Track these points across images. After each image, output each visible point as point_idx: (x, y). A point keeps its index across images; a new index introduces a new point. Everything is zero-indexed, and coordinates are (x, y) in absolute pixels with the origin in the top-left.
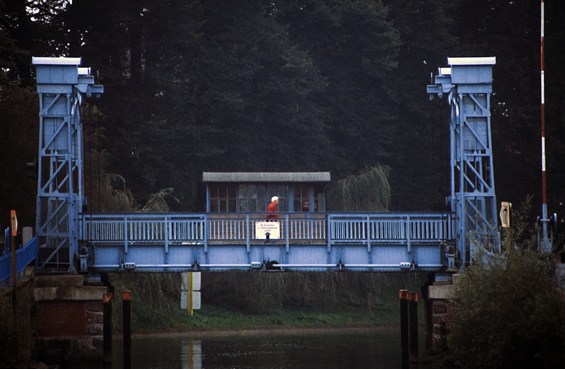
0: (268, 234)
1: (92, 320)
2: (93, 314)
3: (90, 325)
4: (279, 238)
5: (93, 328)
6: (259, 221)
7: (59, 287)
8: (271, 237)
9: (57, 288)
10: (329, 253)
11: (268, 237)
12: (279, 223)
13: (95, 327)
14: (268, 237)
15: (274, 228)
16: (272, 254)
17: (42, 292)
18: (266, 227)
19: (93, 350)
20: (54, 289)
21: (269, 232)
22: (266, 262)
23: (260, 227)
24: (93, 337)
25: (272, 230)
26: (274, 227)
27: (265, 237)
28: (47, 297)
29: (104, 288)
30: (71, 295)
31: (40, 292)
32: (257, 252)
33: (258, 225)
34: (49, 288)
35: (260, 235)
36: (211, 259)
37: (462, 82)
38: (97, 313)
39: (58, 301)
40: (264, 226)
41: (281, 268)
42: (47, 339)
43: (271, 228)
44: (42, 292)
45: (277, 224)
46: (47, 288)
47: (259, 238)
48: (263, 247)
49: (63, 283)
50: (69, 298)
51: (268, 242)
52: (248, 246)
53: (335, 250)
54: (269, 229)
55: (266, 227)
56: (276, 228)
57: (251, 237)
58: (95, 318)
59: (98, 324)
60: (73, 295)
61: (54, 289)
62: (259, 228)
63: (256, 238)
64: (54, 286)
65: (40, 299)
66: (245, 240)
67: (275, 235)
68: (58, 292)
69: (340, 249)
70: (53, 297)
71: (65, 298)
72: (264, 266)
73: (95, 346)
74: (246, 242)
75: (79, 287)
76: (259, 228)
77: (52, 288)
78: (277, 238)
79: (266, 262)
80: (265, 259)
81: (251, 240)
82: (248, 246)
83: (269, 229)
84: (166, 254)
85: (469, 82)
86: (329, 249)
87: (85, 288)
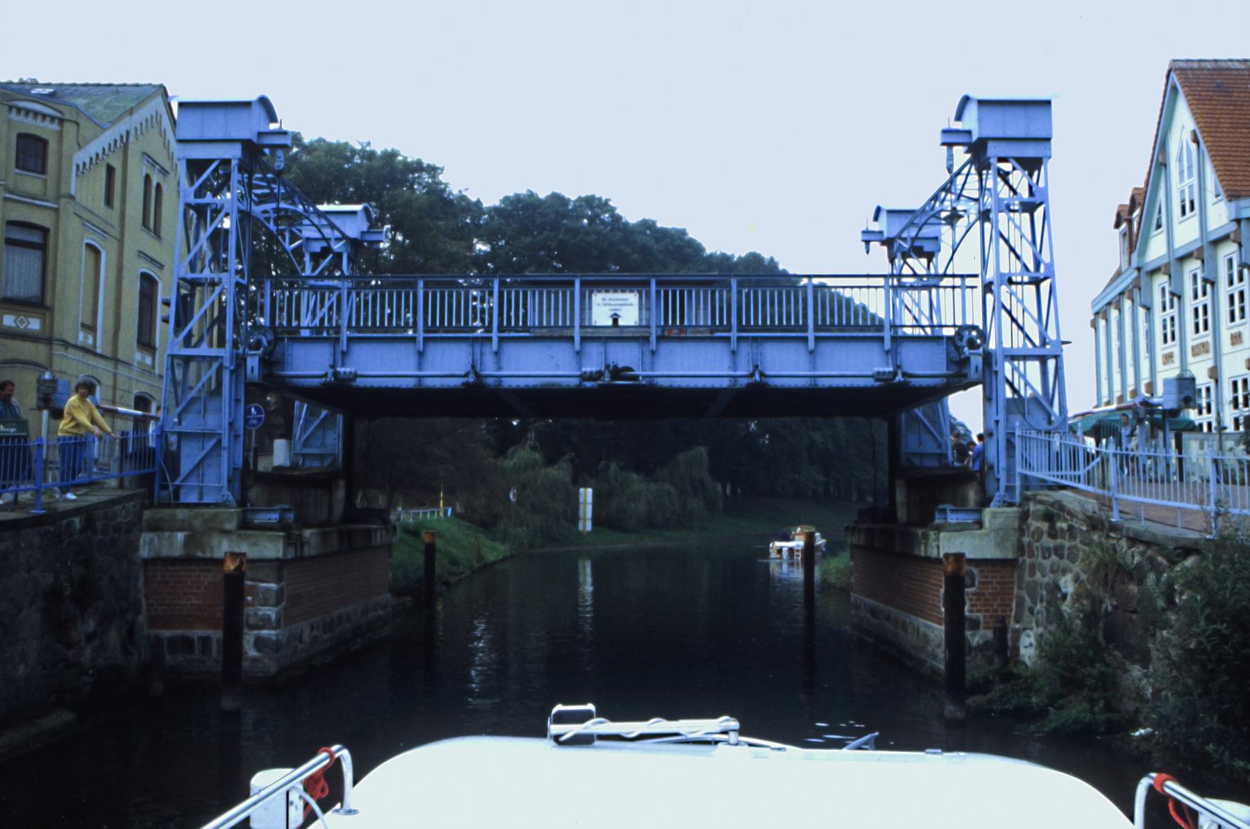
0: (615, 317)
1: (253, 599)
2: (256, 587)
3: (251, 608)
4: (638, 324)
5: (256, 614)
6: (599, 291)
7: (190, 532)
8: (621, 323)
9: (186, 533)
10: (734, 353)
11: (615, 321)
12: (638, 295)
13: (260, 613)
14: (615, 321)
15: (626, 305)
16: (625, 356)
17: (156, 540)
18: (613, 302)
19: (254, 660)
20: (180, 536)
21: (619, 313)
22: (611, 368)
23: (601, 302)
24: (255, 632)
25: (624, 308)
26: (628, 302)
27: (610, 323)
28: (165, 552)
29: (278, 536)
30: (212, 549)
31: (152, 541)
32: (594, 350)
33: (598, 298)
34: (170, 533)
35: (601, 315)
36: (504, 364)
37: (999, 134)
38: (264, 585)
39: (188, 560)
40: (607, 302)
41: (640, 378)
42: (166, 633)
43: (621, 305)
44: (156, 540)
45: (632, 298)
46: (167, 534)
47: (598, 324)
48: (605, 342)
49: (197, 523)
50: (208, 555)
51: (616, 334)
52: (577, 339)
53: (745, 349)
54: (618, 307)
55: (613, 302)
56: (631, 305)
57: (582, 319)
58: (261, 596)
59: (266, 608)
60: (216, 549)
61: (180, 536)
62: (599, 305)
63: (593, 324)
64: (181, 530)
65: (152, 554)
66: (572, 326)
67: (630, 316)
68: (188, 542)
69: (755, 345)
70: (178, 552)
71: (200, 554)
72: (607, 374)
73: (259, 650)
74: (573, 332)
75: (227, 533)
76: (599, 305)
77: (175, 533)
78: (632, 324)
79: (611, 368)
80: (608, 363)
81: (582, 327)
82: (577, 339)
83: (618, 307)
84: (421, 354)
85: (1011, 134)
86: (734, 345)
87: (239, 535)
